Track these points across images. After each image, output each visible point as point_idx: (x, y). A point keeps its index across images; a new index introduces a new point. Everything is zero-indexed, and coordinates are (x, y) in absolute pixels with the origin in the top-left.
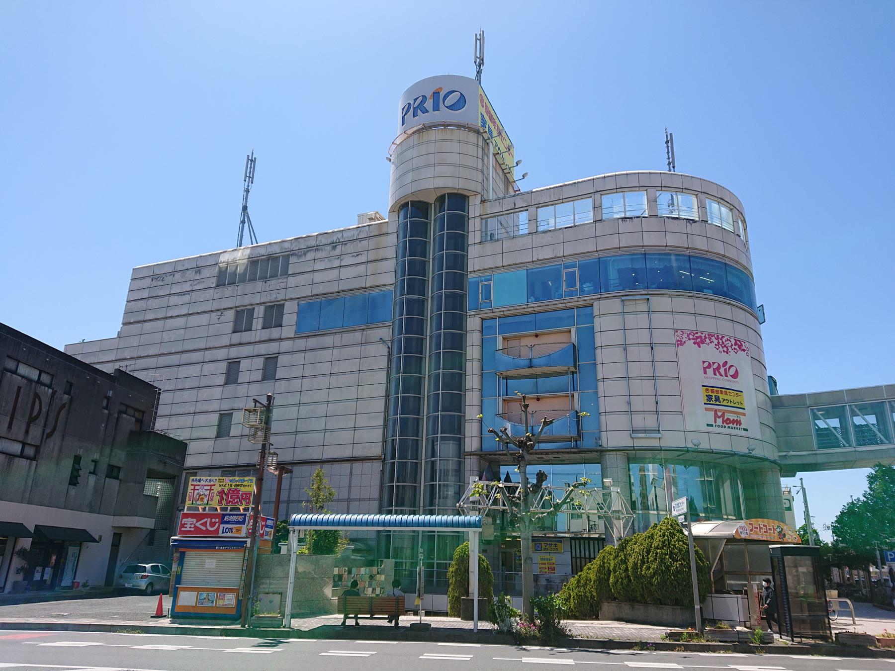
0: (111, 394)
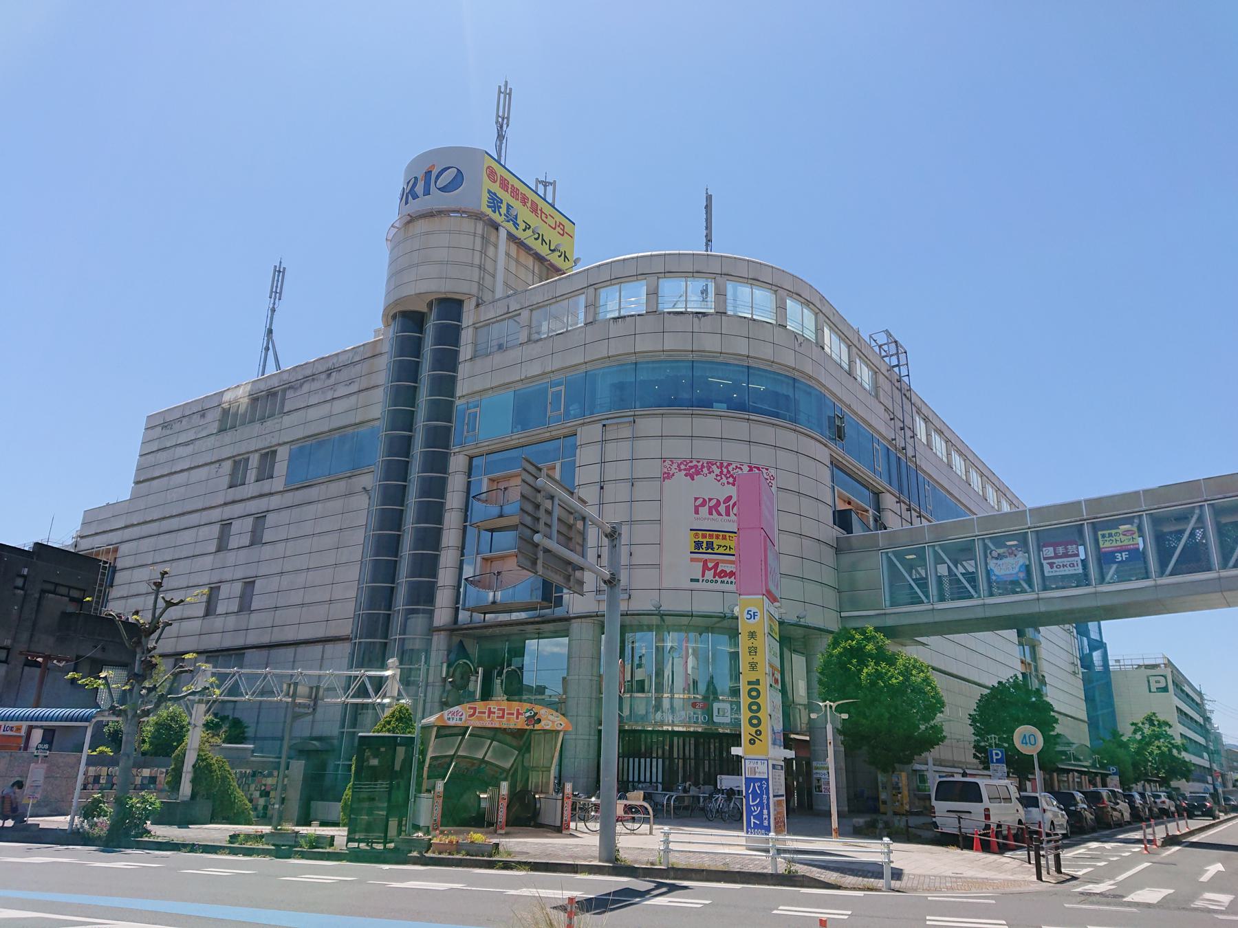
0: (25, 571)
